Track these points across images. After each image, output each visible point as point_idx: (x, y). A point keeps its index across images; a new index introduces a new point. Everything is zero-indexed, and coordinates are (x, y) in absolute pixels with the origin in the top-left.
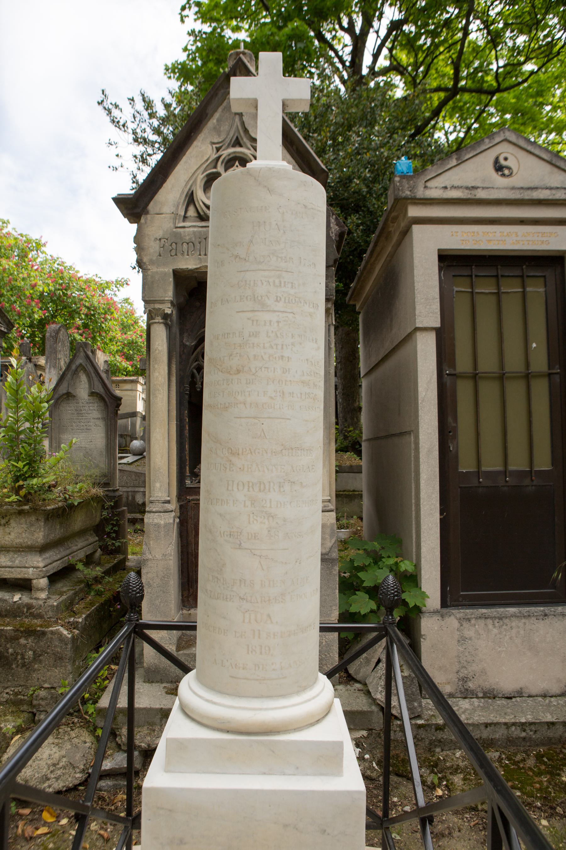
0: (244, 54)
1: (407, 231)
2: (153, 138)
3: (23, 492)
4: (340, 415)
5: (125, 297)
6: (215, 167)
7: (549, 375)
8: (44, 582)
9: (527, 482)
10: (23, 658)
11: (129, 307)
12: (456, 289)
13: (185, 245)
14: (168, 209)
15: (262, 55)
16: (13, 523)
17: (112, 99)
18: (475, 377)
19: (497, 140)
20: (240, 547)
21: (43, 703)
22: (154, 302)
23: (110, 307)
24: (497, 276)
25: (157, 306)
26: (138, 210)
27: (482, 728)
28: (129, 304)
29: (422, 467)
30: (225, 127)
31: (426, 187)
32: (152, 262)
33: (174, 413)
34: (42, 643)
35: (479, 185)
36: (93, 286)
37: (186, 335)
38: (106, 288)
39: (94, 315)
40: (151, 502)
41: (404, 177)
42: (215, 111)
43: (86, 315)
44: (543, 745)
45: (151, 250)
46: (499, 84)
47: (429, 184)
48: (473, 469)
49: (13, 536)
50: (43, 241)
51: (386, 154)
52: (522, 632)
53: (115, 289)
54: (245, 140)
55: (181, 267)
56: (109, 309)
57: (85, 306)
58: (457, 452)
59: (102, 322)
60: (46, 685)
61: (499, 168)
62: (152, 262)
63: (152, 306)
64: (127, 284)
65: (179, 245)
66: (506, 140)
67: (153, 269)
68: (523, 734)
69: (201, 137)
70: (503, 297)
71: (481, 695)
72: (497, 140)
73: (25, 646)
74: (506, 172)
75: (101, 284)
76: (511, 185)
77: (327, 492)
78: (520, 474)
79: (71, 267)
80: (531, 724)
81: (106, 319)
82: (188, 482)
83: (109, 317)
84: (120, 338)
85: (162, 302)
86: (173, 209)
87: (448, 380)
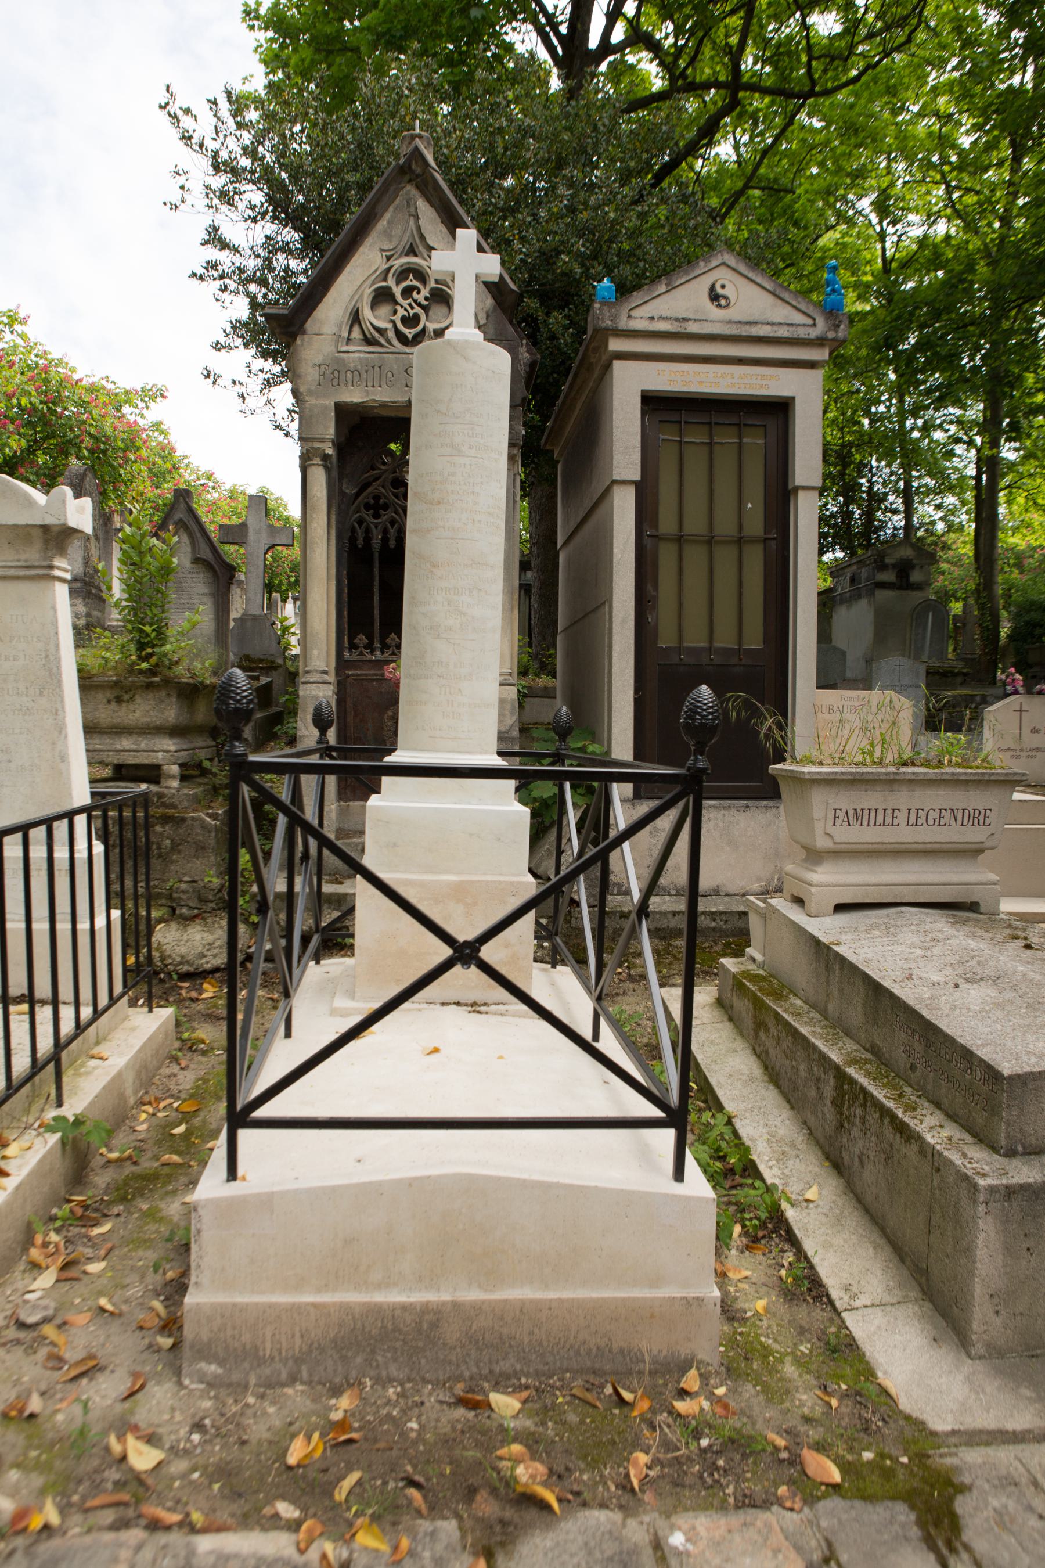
0: (420, 137)
1: (608, 367)
2: (245, 162)
3: (154, 660)
4: (535, 630)
5: (155, 420)
6: (385, 280)
7: (765, 540)
8: (175, 769)
9: (734, 661)
10: (159, 848)
11: (161, 438)
12: (662, 437)
13: (349, 374)
14: (329, 329)
15: (458, 231)
16: (138, 699)
17: (182, 101)
18: (680, 540)
19: (714, 263)
20: (439, 637)
21: (184, 896)
22: (313, 440)
23: (132, 441)
24: (710, 423)
25: (317, 445)
26: (293, 329)
27: (670, 916)
28: (162, 432)
29: (615, 638)
30: (397, 231)
31: (629, 316)
32: (310, 392)
33: (333, 571)
34: (181, 831)
35: (691, 316)
36: (103, 399)
37: (345, 480)
38: (126, 402)
39: (105, 452)
40: (307, 672)
41: (604, 303)
42: (386, 210)
43: (91, 451)
44: (734, 936)
45: (310, 379)
46: (813, 83)
47: (633, 313)
48: (673, 644)
49: (138, 714)
50: (22, 315)
51: (612, 215)
52: (721, 824)
53: (141, 405)
54: (421, 249)
55: (348, 400)
56: (133, 441)
57: (90, 434)
58: (656, 625)
59: (120, 466)
60: (186, 879)
61: (714, 297)
62: (310, 392)
63: (310, 444)
64: (163, 396)
65: (342, 373)
66: (724, 264)
67: (311, 401)
68: (713, 924)
69: (369, 241)
70: (717, 449)
71: (673, 892)
72: (714, 263)
73: (161, 834)
74: (723, 302)
75: (116, 395)
76: (727, 318)
77: (508, 664)
78: (726, 651)
79: (60, 361)
80: (721, 913)
81: (126, 460)
82: (346, 654)
83: (132, 457)
84: (150, 495)
85: (322, 440)
86: (335, 330)
87: (648, 543)
